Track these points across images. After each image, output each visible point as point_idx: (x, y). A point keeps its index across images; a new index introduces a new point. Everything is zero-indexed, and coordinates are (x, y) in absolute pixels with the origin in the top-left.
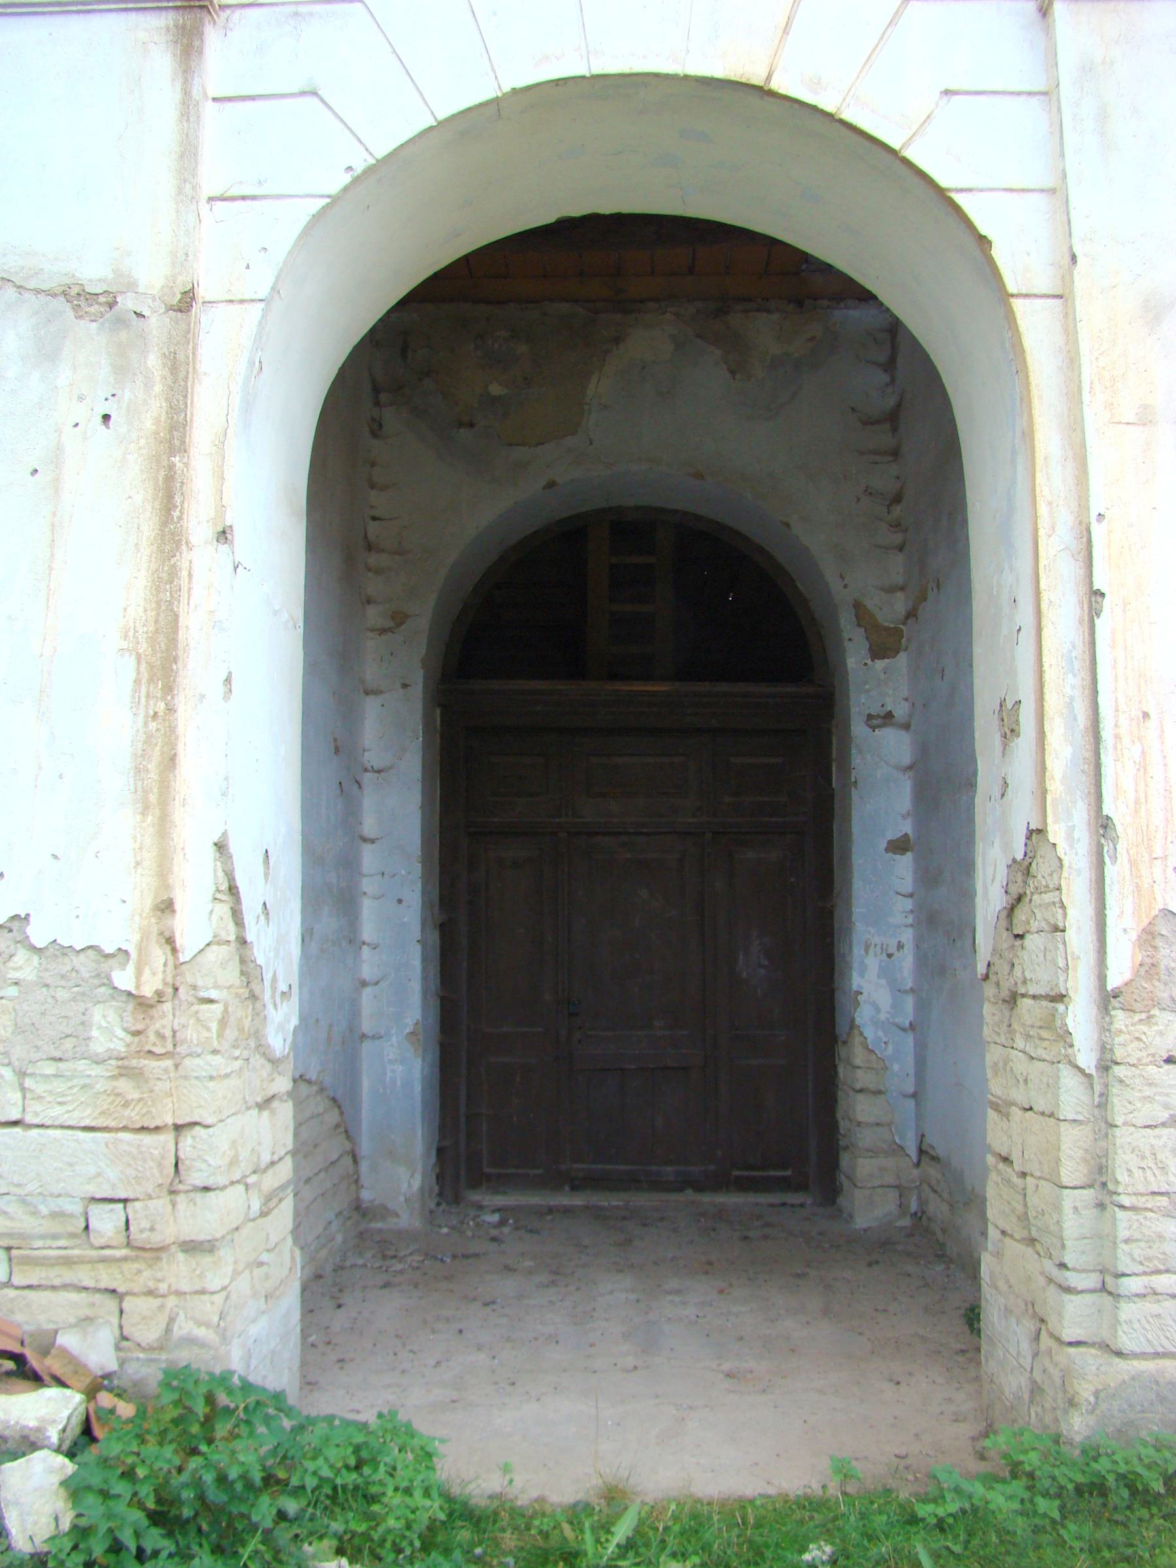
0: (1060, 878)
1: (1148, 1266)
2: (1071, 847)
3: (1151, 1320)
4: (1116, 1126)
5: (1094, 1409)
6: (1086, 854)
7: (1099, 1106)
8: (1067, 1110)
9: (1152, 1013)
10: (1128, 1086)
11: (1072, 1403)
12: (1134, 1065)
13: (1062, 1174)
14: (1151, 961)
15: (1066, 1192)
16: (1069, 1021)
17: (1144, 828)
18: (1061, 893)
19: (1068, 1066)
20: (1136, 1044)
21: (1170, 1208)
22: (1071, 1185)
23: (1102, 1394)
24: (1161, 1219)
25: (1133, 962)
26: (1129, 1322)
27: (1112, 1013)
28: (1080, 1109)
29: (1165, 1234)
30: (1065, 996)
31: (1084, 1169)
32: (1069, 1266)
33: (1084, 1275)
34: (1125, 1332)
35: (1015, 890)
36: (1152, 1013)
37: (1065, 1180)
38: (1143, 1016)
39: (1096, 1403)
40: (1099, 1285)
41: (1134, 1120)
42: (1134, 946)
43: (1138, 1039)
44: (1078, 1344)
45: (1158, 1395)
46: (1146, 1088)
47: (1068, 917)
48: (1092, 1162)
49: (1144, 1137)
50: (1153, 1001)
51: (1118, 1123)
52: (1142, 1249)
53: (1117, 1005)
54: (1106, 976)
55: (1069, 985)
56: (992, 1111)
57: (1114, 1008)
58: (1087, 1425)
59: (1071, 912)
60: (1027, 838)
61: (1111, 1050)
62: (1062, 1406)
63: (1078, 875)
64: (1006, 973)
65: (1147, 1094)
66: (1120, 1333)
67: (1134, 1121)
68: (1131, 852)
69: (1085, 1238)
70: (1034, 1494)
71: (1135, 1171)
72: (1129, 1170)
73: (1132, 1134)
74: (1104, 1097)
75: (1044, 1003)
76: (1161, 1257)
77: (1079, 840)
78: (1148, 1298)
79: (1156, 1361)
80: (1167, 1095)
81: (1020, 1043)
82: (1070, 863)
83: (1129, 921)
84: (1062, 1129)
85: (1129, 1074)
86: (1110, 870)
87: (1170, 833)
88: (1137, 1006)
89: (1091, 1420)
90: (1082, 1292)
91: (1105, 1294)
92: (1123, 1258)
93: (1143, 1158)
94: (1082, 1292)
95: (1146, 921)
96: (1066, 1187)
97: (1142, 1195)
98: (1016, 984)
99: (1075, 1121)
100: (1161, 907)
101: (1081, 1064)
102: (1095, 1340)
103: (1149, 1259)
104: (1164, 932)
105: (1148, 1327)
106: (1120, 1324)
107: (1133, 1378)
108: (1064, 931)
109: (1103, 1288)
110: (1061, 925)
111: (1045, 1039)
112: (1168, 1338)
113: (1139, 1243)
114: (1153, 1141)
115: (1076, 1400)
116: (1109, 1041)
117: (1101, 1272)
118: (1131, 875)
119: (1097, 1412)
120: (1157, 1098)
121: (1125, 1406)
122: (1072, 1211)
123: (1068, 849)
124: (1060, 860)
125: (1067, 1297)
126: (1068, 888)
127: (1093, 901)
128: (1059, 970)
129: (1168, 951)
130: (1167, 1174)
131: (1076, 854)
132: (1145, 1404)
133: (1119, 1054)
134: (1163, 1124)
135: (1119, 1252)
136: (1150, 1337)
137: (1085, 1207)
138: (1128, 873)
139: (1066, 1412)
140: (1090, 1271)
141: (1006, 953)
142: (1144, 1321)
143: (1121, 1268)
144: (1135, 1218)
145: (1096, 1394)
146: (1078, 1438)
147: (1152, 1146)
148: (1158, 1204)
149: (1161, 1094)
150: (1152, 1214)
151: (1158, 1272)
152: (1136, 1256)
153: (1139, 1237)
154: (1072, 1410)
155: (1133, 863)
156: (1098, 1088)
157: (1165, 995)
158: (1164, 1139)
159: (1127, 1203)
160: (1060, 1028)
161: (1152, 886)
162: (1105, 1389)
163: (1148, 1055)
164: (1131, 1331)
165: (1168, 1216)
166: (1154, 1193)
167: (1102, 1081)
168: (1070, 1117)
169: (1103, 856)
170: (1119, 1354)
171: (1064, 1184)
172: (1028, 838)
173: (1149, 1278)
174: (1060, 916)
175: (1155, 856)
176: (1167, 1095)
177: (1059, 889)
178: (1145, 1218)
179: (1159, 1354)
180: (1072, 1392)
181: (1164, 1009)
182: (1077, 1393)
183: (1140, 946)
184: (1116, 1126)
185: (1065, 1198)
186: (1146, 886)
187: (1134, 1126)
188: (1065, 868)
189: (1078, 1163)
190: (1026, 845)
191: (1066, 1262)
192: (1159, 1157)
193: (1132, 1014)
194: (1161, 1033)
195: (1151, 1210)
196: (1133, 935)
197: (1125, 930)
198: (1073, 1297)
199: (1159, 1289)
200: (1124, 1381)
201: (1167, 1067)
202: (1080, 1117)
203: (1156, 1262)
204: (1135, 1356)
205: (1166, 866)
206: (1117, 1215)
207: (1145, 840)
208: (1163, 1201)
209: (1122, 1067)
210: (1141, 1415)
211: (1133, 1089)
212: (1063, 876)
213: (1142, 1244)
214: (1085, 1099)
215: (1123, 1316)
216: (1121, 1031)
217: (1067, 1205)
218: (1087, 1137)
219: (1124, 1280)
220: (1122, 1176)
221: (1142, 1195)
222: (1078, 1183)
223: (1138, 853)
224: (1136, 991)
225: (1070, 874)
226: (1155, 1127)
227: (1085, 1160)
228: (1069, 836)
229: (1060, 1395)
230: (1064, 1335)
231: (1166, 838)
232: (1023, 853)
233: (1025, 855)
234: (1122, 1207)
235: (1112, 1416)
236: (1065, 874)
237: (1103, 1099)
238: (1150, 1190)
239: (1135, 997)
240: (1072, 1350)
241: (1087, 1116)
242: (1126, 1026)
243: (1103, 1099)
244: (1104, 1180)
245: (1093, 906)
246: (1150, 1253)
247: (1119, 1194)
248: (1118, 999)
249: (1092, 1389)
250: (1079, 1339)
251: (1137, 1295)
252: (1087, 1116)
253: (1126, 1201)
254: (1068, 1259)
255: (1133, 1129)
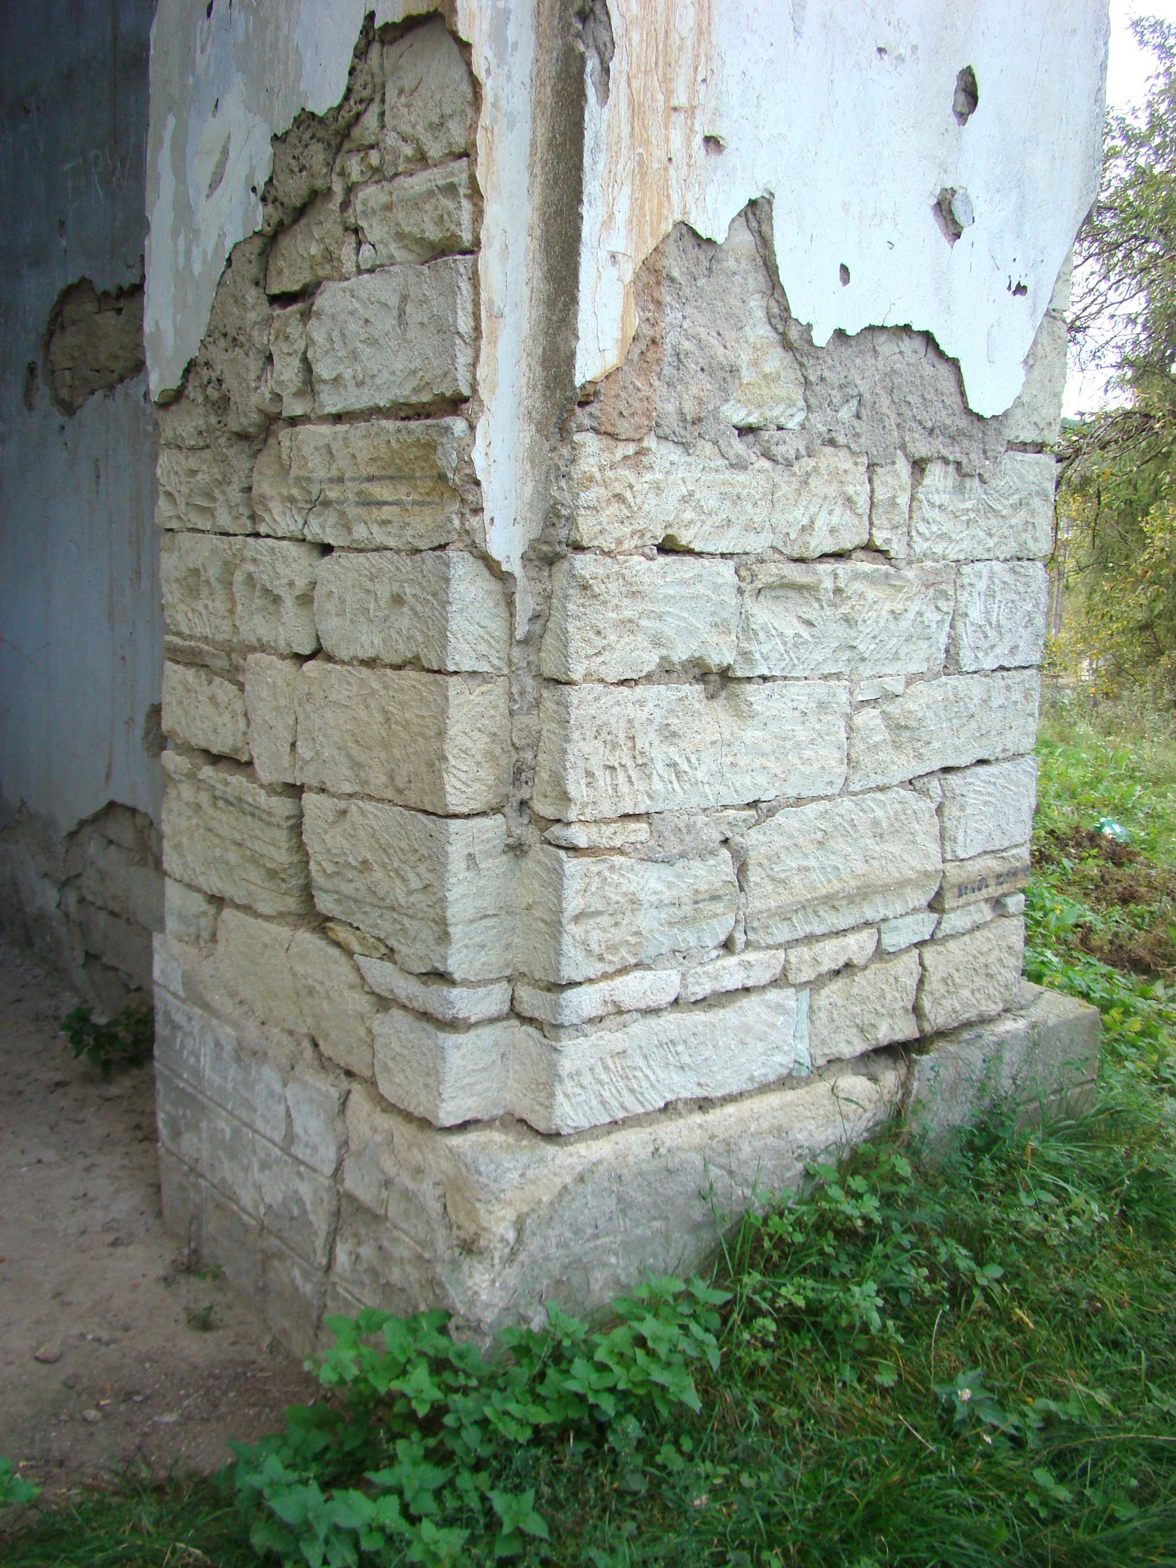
0: (473, 128)
1: (610, 962)
2: (500, 56)
3: (610, 1062)
4: (569, 683)
5: (514, 1253)
6: (527, 81)
7: (525, 642)
8: (462, 656)
9: (645, 444)
10: (595, 596)
11: (469, 1247)
12: (608, 554)
13: (448, 788)
14: (651, 333)
15: (455, 825)
16: (477, 457)
17: (661, 36)
18: (473, 163)
19: (467, 555)
20: (614, 508)
21: (652, 843)
22: (466, 810)
23: (528, 1221)
24: (637, 867)
25: (623, 328)
26: (576, 1075)
27: (577, 438)
28: (483, 648)
29: (641, 896)
30: (466, 400)
31: (487, 774)
32: (457, 976)
33: (482, 991)
34: (566, 1095)
35: (294, 189)
36: (645, 444)
37: (455, 801)
38: (631, 449)
39: (519, 1239)
40: (506, 1008)
41: (603, 669)
42: (627, 294)
43: (619, 497)
44: (464, 1127)
45: (620, 1199)
46: (626, 602)
47: (488, 218)
48: (504, 760)
49: (618, 703)
50: (649, 418)
51: (576, 676)
52: (605, 930)
53: (587, 422)
54: (573, 355)
55: (481, 372)
56: (180, 668)
57: (581, 429)
58: (504, 1287)
59: (492, 209)
60: (356, 56)
61: (571, 520)
62: (447, 1255)
63: (511, 127)
64: (253, 376)
65: (628, 614)
66: (560, 1098)
67: (603, 672)
68: (635, 84)
69: (486, 916)
70: (457, 1471)
71: (599, 773)
72: (589, 774)
73: (597, 699)
74: (541, 621)
75: (390, 425)
76: (632, 940)
77: (515, 46)
78: (607, 1023)
79: (613, 1137)
80: (660, 617)
81: (283, 520)
82: (496, 97)
83: (619, 241)
84: (452, 693)
85: (601, 571)
86: (596, 117)
87: (703, 60)
88: (624, 428)
89: (511, 1275)
90: (477, 1024)
91: (515, 1022)
92: (573, 951)
93: (615, 746)
94: (477, 1024)
95: (651, 244)
96: (455, 816)
97: (607, 821)
98: (278, 398)
99: (474, 673)
100: (678, 217)
101: (496, 550)
102: (495, 1112)
103: (613, 948)
104: (675, 274)
105: (604, 1077)
106: (561, 1081)
107: (581, 1179)
108: (473, 249)
109: (514, 1013)
110: (467, 237)
111: (385, 503)
112: (632, 1091)
113: (598, 920)
114: (630, 711)
115: (482, 1243)
116: (568, 500)
117: (509, 979)
118: (632, 135)
119: (522, 1256)
120: (644, 623)
121: (568, 1235)
122: (463, 865)
123: (493, 61)
124: (475, 84)
125: (450, 1039)
126: (489, 154)
127: (537, 189)
128: (458, 341)
129: (679, 315)
130: (649, 777)
131: (509, 78)
132: (601, 1223)
133: (586, 528)
134: (649, 678)
135: (566, 939)
136: (606, 1094)
137: (488, 855)
138: (625, 130)
139: (455, 1265)
140: (492, 981)
141: (255, 333)
142: (599, 1069)
143: (568, 972)
144: (595, 869)
145: (519, 1226)
146: (489, 1317)
147: (630, 721)
148: (632, 839)
149: (649, 614)
150: (622, 859)
151: (624, 970)
152: (594, 947)
153: (600, 908)
154: (467, 1263)
155: (636, 110)
156: (526, 604)
157: (670, 408)
158: (650, 705)
159: (582, 843)
160: (456, 470)
161: (666, 169)
162: (533, 1210)
163: (633, 533)
164: (578, 1090)
165: (650, 860)
166: (626, 816)
167: (539, 587)
168: (467, 665)
169: (582, 82)
170: (553, 1137)
171: (452, 809)
172: (361, 53)
173: (612, 983)
174: (466, 217)
175: (675, 102)
176: (660, 617)
177: (467, 153)
178: (612, 868)
179: (616, 1122)
180: (473, 1228)
181: (666, 438)
182: (485, 1229)
183: (637, 295)
184: (569, 683)
185: (452, 838)
186: (656, 166)
187: (601, 681)
188: (486, 107)
189: (478, 764)
190: (352, 72)
191: (450, 969)
192: (639, 745)
193: (611, 442)
194: (657, 488)
195: (620, 851)
196: (628, 270)
197: (613, 257)
198: (460, 1038)
199: (627, 1003)
200: (565, 1187)
201: (662, 559)
202: (484, 667)
203: (623, 952)
204: (581, 1134)
205: (691, 129)
206: (566, 867)
207: (661, 63)
208: (639, 831)
209: (588, 557)
210: (591, 1244)
211: (604, 603)
212: (481, 123)
213: (605, 920)
214: (497, 627)
215: (566, 1065)
216: (591, 479)
217: (456, 852)
218: (495, 707)
219: (571, 994)
220: (576, 788)
221: (607, 821)
222: (478, 806)
223: (646, 89)
224: (623, 395)
225: (495, 121)
226: (636, 682)
227: (491, 757)
228: (498, 34)
229: (441, 1233)
230: (442, 1115)
231: (696, 68)
232: (342, 91)
233: (346, 98)
234: (573, 849)
235: (547, 1259)
236: (485, 120)
237: (537, 627)
238: (620, 812)
239: (622, 406)
240: (455, 1141)
241: (496, 662)
242: (601, 469)
243: (537, 627)
244: (525, 793)
245: (537, 200)
246: (617, 935)
247: (569, 824)
248: (588, 409)
249: (511, 1215)
250: (469, 1116)
251: (591, 1021)
252: (496, 662)
253: (580, 836)
254: (457, 962)
255: (599, 687)
